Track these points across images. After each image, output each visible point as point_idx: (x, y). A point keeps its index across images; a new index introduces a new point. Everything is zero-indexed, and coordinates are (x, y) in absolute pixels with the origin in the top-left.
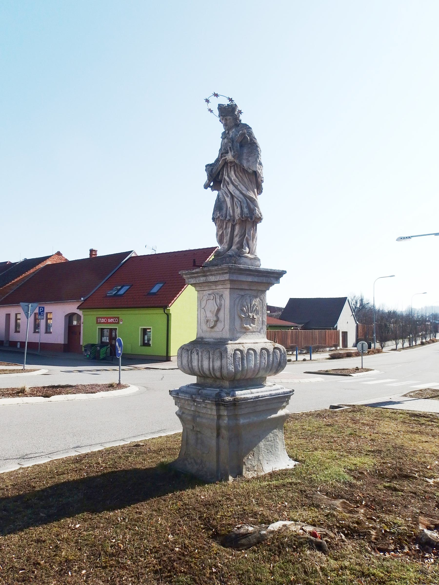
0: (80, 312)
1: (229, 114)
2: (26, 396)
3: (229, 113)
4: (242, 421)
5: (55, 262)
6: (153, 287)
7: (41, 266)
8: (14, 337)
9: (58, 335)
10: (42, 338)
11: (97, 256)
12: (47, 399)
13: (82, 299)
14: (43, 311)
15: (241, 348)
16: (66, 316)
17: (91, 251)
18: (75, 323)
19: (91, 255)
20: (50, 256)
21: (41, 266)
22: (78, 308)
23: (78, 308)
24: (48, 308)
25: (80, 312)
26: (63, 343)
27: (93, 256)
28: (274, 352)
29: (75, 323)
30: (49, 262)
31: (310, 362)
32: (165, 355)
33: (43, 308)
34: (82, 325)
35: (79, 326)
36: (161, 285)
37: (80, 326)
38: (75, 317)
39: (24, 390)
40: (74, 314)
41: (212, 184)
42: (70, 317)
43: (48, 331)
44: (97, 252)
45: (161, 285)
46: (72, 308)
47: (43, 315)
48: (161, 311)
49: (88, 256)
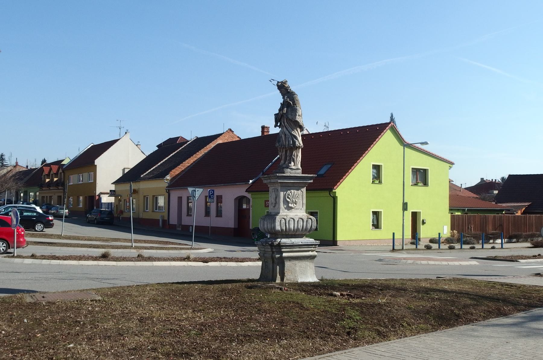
0: (249, 195)
1: (283, 87)
2: (190, 261)
3: (283, 87)
4: (284, 255)
5: (226, 141)
6: (321, 168)
7: (212, 145)
8: (186, 221)
9: (228, 219)
10: (214, 222)
11: (270, 133)
12: (206, 264)
13: (251, 181)
14: (213, 194)
15: (285, 217)
16: (236, 199)
17: (263, 128)
18: (245, 206)
19: (263, 132)
20: (221, 134)
21: (212, 145)
22: (247, 191)
23: (247, 191)
24: (218, 191)
25: (249, 195)
26: (233, 227)
27: (265, 134)
28: (307, 221)
29: (245, 206)
30: (219, 141)
31: (482, 250)
32: (332, 239)
33: (213, 191)
34: (251, 208)
35: (248, 210)
36: (329, 166)
37: (249, 209)
38: (244, 200)
39: (189, 257)
40: (244, 197)
41: (279, 124)
42: (240, 200)
43: (219, 214)
44: (270, 129)
45: (329, 166)
46: (240, 191)
47: (213, 198)
48: (326, 193)
49: (260, 135)
